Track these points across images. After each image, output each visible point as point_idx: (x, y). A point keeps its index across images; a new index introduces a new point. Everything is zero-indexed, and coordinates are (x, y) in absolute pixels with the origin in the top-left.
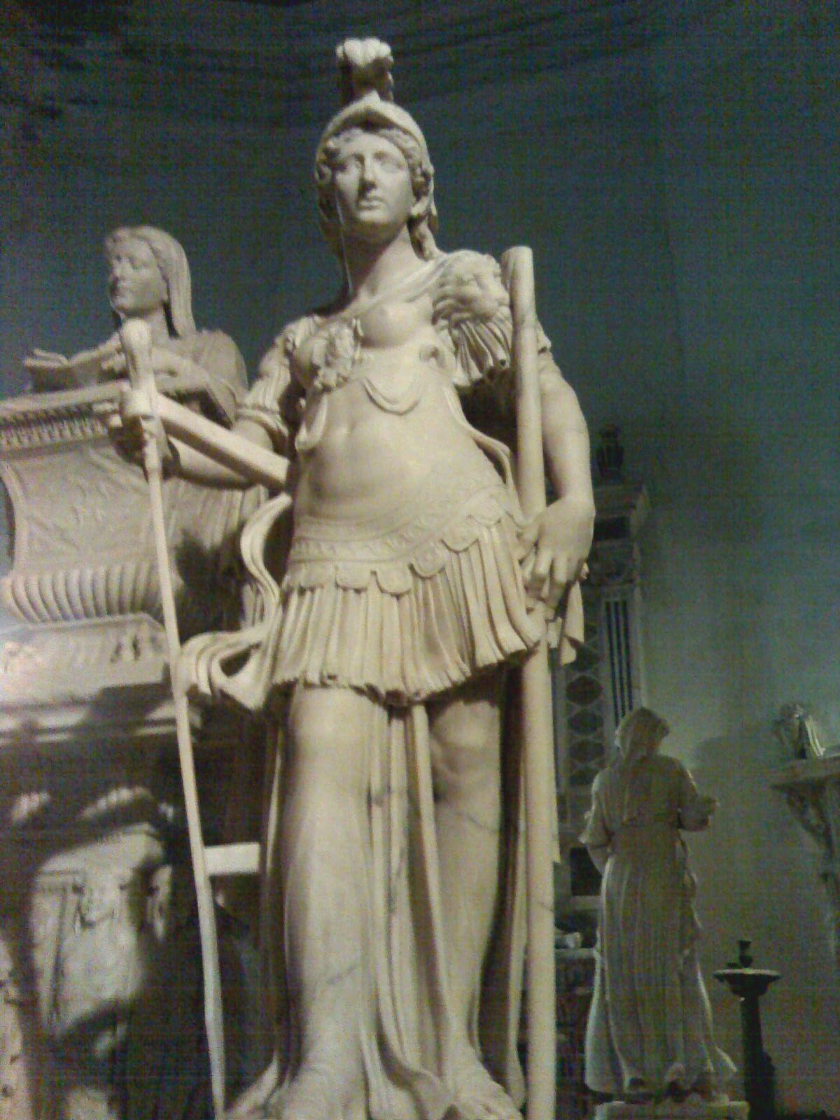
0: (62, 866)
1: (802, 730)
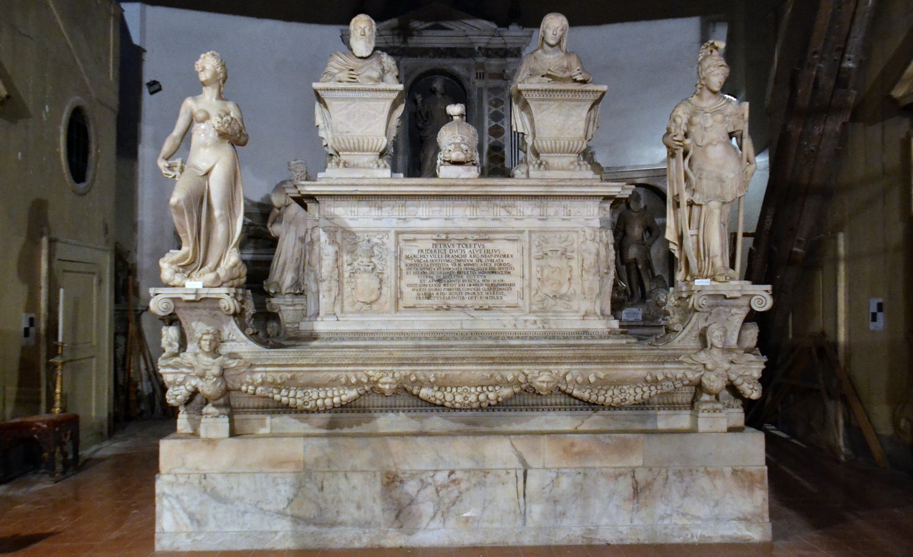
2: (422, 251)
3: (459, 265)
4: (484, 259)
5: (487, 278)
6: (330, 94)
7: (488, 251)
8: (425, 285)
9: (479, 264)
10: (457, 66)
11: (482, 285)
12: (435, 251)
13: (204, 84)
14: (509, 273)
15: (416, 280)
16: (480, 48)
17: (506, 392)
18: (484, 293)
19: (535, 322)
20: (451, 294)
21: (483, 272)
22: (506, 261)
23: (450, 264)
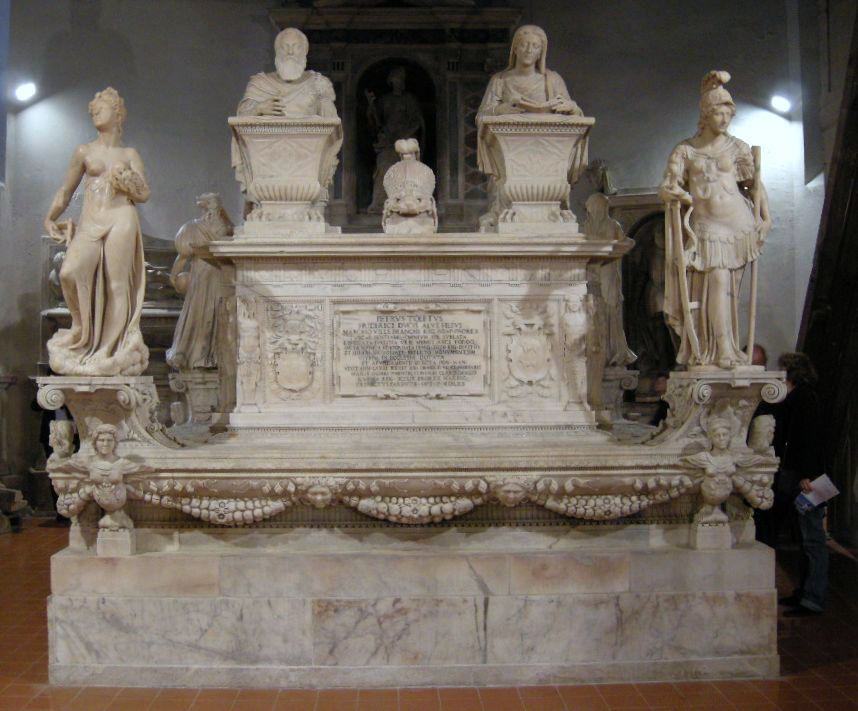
0: (558, 292)
1: (604, 176)
2: (364, 325)
4: (441, 336)
6: (249, 130)
10: (423, 56)
13: (610, 244)
15: (355, 361)
16: (452, 30)
17: (465, 503)
19: (505, 414)
21: (440, 352)
22: (470, 337)
23: (398, 341)
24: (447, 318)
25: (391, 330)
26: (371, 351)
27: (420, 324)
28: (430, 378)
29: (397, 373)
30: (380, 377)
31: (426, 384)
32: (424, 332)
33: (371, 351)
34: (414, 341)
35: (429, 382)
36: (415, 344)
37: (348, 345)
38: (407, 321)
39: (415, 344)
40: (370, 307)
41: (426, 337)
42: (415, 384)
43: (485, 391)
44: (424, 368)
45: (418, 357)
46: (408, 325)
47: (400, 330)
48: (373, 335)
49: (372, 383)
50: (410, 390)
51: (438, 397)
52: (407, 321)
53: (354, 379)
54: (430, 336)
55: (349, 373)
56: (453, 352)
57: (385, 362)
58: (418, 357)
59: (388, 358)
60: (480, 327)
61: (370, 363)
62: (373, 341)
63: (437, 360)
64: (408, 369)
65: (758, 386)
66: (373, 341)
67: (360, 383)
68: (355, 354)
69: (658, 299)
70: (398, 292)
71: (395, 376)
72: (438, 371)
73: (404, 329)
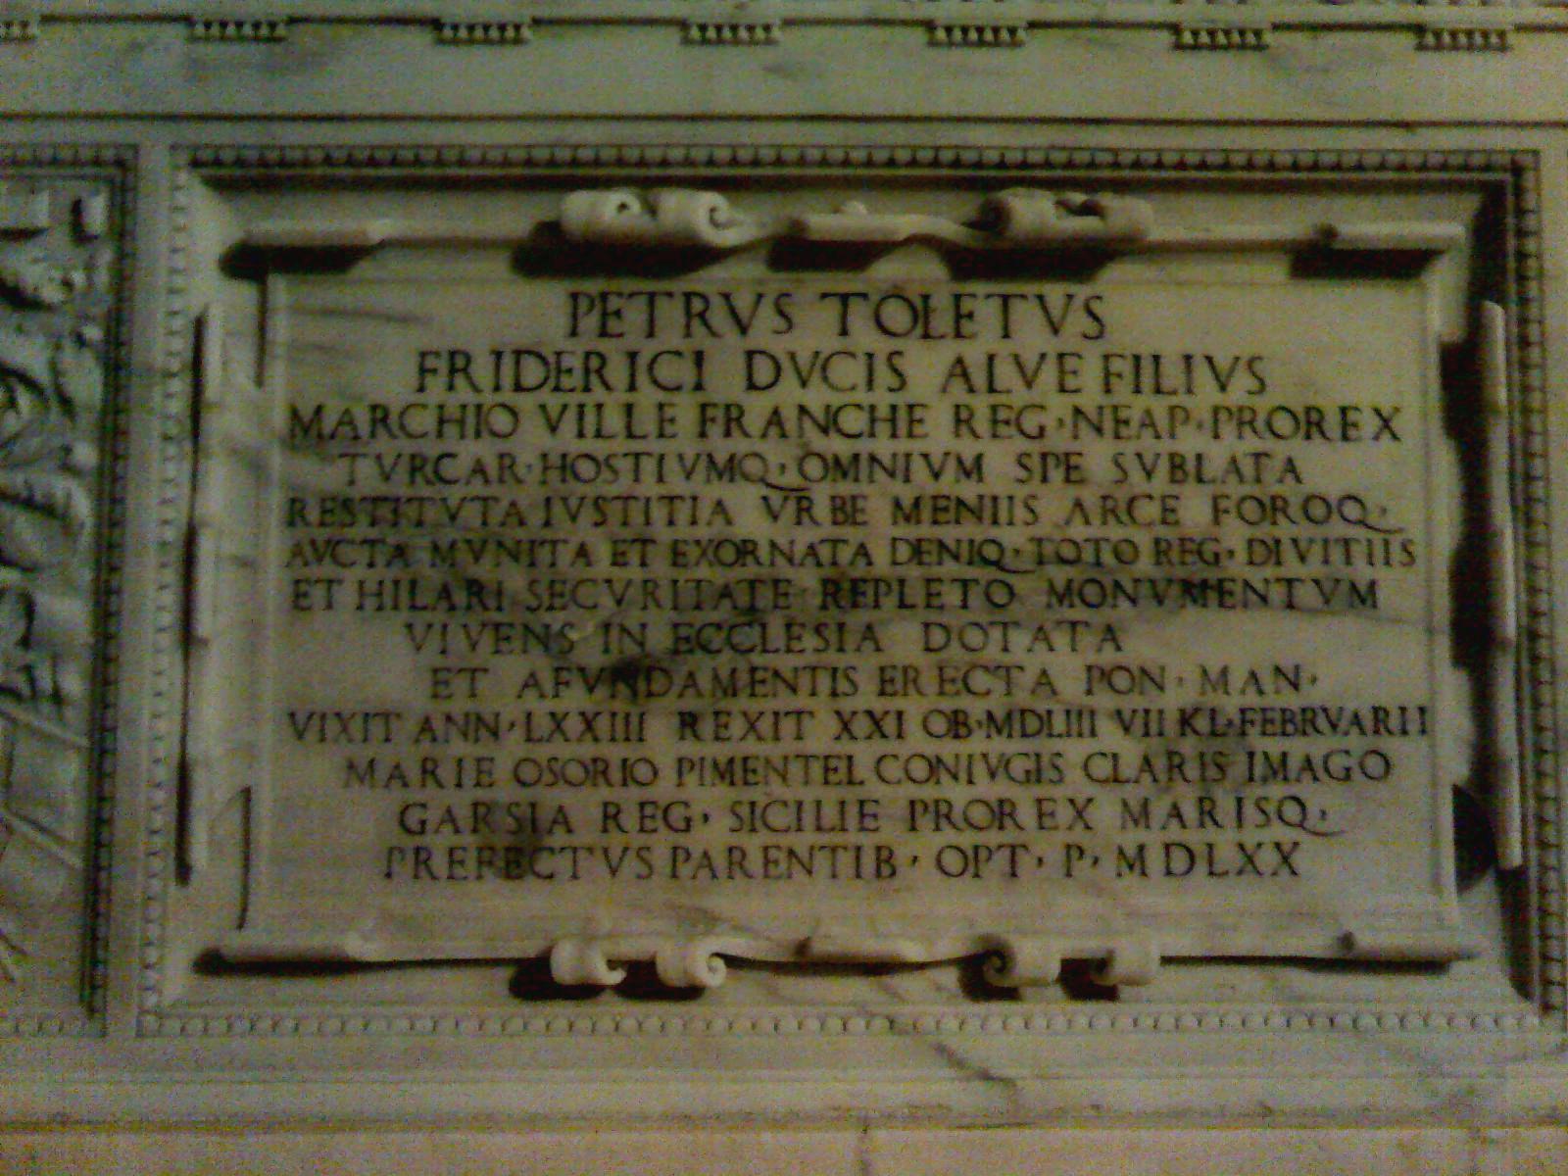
2: (458, 364)
3: (846, 511)
4: (1097, 455)
5: (1141, 647)
7: (1146, 369)
8: (483, 726)
9: (1054, 501)
11: (1082, 720)
12: (595, 367)
14: (1364, 597)
15: (380, 662)
18: (1106, 811)
20: (752, 818)
21: (1090, 588)
22: (1327, 467)
24: (1140, 307)
25: (685, 411)
26: (515, 579)
27: (926, 365)
28: (1002, 813)
29: (726, 772)
30: (585, 804)
31: (973, 861)
32: (962, 420)
33: (515, 579)
34: (877, 497)
35: (989, 851)
36: (880, 530)
37: (316, 534)
38: (815, 330)
39: (880, 530)
40: (513, 217)
41: (973, 469)
42: (886, 863)
43: (1468, 920)
44: (958, 724)
45: (903, 640)
46: (823, 364)
47: (757, 408)
48: (532, 442)
49: (518, 851)
50: (845, 919)
51: (1086, 979)
52: (815, 330)
53: (367, 816)
54: (1000, 459)
55: (321, 767)
56: (1196, 591)
57: (630, 674)
58: (903, 640)
59: (659, 639)
60: (1412, 389)
61: (506, 680)
62: (528, 496)
63: (1067, 666)
64: (821, 736)
65: (62, 848)
66: (528, 496)
67: (410, 855)
68: (374, 600)
69: (1499, 654)
70: (735, 82)
71: (709, 796)
72: (1075, 750)
73: (788, 394)
